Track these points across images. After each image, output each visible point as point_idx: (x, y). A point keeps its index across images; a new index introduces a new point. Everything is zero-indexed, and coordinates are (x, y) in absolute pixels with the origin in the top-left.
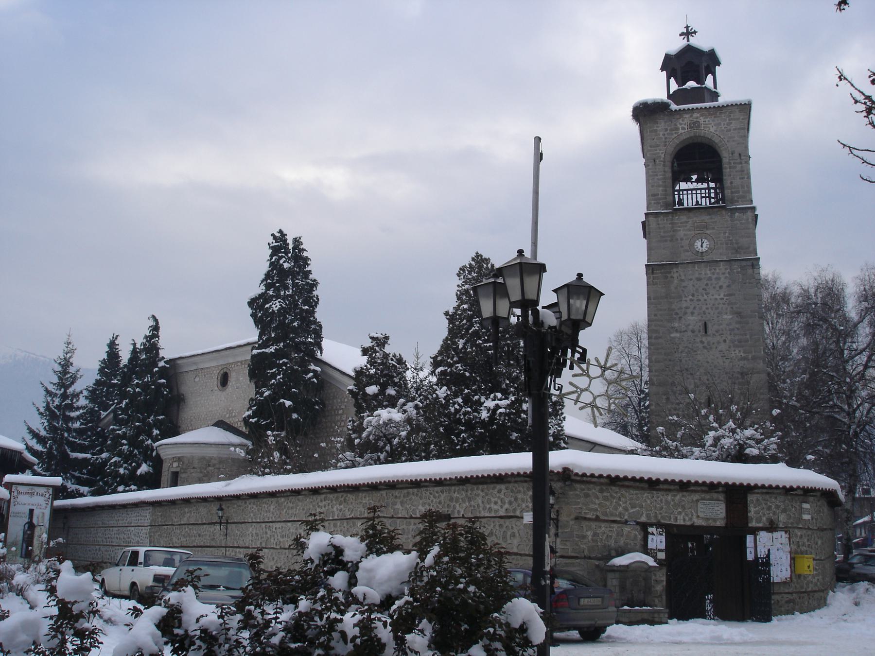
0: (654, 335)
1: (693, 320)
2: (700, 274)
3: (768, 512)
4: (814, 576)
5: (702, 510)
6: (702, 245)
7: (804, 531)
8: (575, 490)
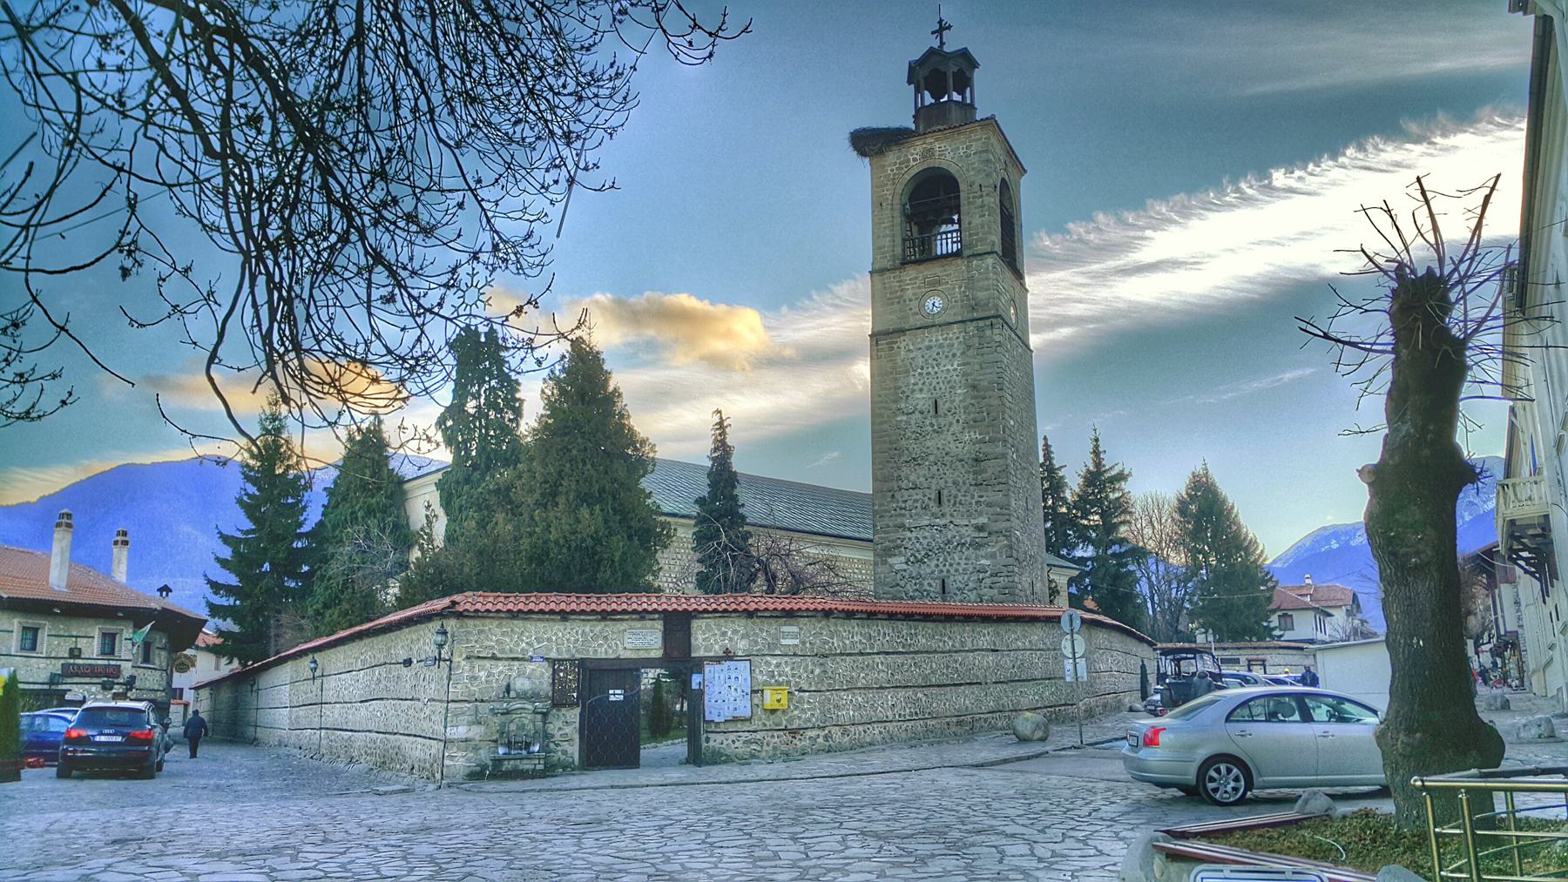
0: (879, 420)
1: (922, 399)
2: (931, 341)
6: (934, 304)
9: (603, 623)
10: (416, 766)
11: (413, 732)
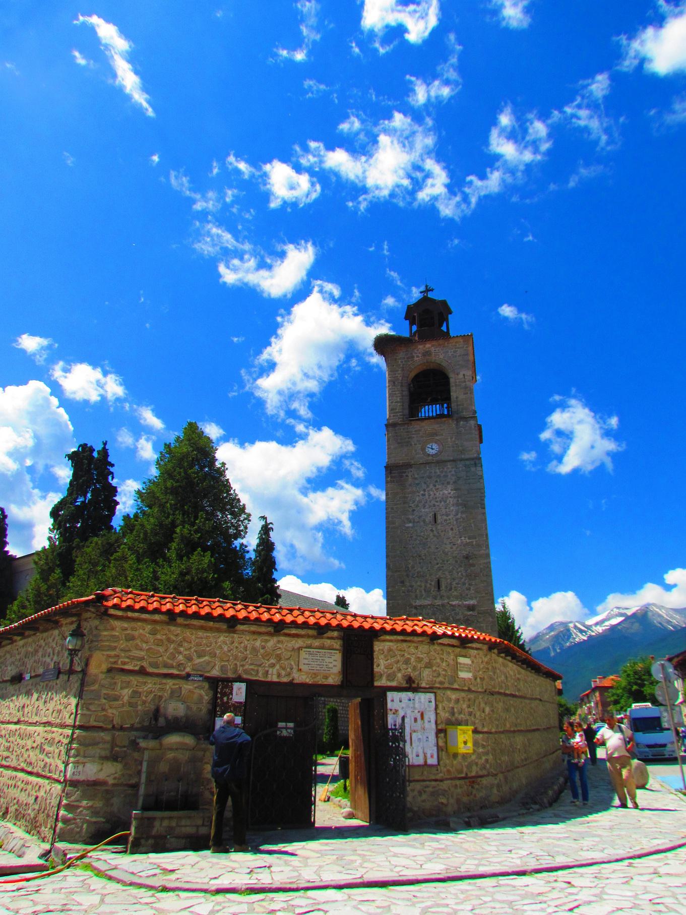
1: (426, 513)
3: (405, 666)
4: (479, 756)
5: (306, 661)
6: (433, 449)
7: (463, 694)
8: (113, 629)
9: (275, 639)
10: (12, 809)
11: (14, 763)
